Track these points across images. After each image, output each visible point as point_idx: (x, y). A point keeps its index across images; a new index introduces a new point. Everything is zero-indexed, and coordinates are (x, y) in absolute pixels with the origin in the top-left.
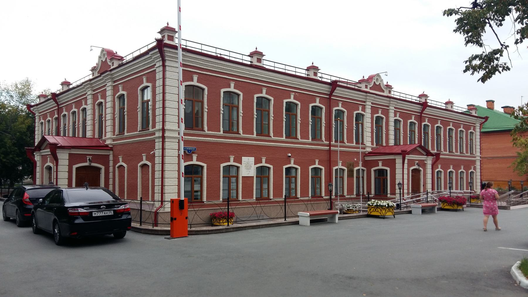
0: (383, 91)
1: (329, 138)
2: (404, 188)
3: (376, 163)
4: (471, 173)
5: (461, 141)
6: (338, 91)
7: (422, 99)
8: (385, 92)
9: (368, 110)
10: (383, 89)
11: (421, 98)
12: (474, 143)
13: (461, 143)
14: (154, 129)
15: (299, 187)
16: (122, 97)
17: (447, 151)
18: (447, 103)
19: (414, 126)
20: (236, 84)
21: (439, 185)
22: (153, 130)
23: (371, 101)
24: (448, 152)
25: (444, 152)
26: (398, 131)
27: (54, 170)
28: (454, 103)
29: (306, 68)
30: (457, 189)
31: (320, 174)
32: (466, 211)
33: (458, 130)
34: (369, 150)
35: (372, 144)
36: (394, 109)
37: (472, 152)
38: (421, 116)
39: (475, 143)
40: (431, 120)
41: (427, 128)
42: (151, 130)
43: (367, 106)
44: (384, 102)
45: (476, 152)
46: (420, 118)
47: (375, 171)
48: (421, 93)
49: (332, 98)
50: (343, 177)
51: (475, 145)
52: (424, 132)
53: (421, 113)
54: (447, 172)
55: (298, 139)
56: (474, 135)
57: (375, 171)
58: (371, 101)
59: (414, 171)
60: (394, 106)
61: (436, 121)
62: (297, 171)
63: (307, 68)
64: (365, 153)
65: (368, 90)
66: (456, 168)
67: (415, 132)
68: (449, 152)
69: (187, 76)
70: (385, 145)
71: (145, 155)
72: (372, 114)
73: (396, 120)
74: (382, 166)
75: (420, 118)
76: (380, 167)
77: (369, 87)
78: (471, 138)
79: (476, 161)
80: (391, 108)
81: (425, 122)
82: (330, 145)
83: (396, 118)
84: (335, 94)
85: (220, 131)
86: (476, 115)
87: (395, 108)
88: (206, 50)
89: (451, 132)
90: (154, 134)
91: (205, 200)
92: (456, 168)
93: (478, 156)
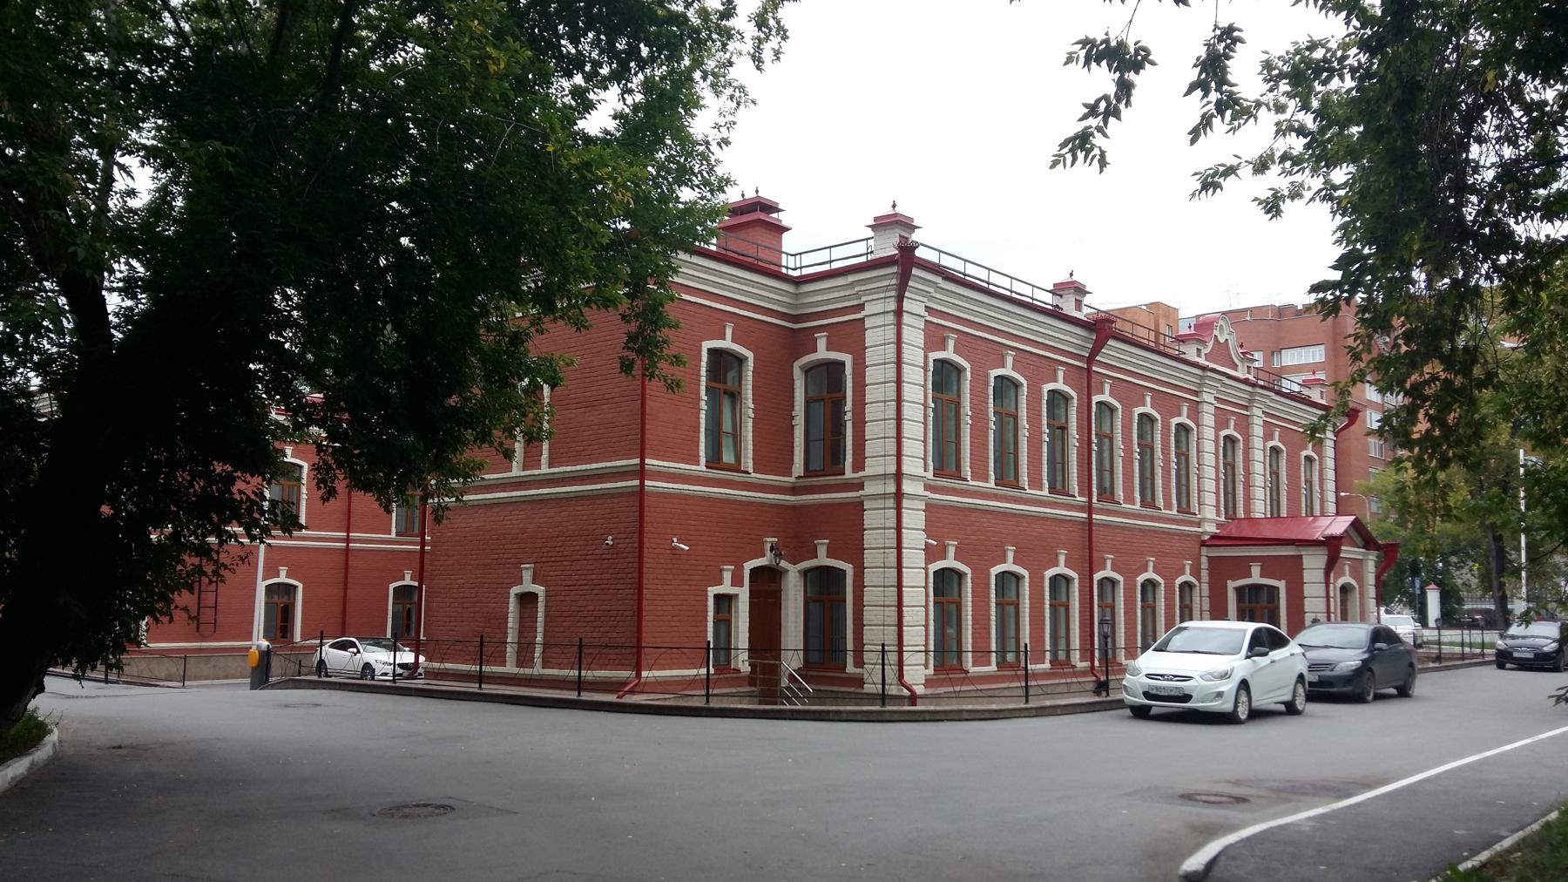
0: (1235, 367)
1: (1086, 489)
2: (905, 638)
3: (1242, 567)
4: (1143, 585)
5: (1106, 448)
6: (1113, 351)
7: (1062, 300)
8: (1240, 368)
9: (1208, 419)
10: (1235, 360)
11: (1061, 296)
12: (1193, 471)
13: (1106, 455)
14: (861, 474)
15: (1028, 627)
16: (1275, 450)
17: (986, 480)
18: (1058, 290)
19: (1063, 406)
20: (1018, 358)
21: (1063, 633)
22: (856, 475)
23: (921, 299)
24: (1046, 492)
25: (1124, 505)
26: (1012, 423)
27: (1335, 601)
28: (1087, 289)
29: (1051, 287)
30: (524, 659)
31: (1014, 592)
32: (1309, 716)
33: (1131, 413)
34: (1211, 528)
35: (1218, 514)
36: (1215, 402)
37: (1231, 512)
38: (1089, 370)
39: (1198, 469)
40: (1119, 387)
41: (954, 378)
42: (849, 474)
43: (1206, 408)
44: (1183, 376)
45: (1199, 504)
46: (1087, 379)
47: (1239, 590)
48: (1063, 277)
49: (1094, 368)
50: (1018, 605)
51: (1199, 478)
52: (999, 409)
53: (1091, 360)
54: (1043, 578)
55: (966, 480)
56: (1194, 437)
57: (1239, 590)
58: (921, 299)
59: (941, 575)
60: (925, 300)
61: (996, 354)
62: (1071, 590)
63: (1055, 285)
64: (1200, 536)
65: (1202, 361)
66: (1036, 556)
67: (1016, 418)
68: (1052, 490)
69: (935, 337)
70: (1243, 516)
71: (953, 545)
72: (1218, 428)
73: (945, 365)
74: (1262, 576)
75: (1087, 379)
76: (1256, 577)
77: (1204, 352)
78: (1275, 468)
79: (862, 503)
80: (1206, 397)
81: (1102, 393)
82: (1090, 509)
83: (1271, 444)
84: (1102, 360)
85: (986, 480)
86: (1323, 402)
87: (927, 308)
88: (1000, 283)
89: (1183, 439)
90: (861, 486)
91: (703, 671)
92: (1036, 556)
93: (1210, 521)
